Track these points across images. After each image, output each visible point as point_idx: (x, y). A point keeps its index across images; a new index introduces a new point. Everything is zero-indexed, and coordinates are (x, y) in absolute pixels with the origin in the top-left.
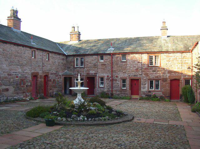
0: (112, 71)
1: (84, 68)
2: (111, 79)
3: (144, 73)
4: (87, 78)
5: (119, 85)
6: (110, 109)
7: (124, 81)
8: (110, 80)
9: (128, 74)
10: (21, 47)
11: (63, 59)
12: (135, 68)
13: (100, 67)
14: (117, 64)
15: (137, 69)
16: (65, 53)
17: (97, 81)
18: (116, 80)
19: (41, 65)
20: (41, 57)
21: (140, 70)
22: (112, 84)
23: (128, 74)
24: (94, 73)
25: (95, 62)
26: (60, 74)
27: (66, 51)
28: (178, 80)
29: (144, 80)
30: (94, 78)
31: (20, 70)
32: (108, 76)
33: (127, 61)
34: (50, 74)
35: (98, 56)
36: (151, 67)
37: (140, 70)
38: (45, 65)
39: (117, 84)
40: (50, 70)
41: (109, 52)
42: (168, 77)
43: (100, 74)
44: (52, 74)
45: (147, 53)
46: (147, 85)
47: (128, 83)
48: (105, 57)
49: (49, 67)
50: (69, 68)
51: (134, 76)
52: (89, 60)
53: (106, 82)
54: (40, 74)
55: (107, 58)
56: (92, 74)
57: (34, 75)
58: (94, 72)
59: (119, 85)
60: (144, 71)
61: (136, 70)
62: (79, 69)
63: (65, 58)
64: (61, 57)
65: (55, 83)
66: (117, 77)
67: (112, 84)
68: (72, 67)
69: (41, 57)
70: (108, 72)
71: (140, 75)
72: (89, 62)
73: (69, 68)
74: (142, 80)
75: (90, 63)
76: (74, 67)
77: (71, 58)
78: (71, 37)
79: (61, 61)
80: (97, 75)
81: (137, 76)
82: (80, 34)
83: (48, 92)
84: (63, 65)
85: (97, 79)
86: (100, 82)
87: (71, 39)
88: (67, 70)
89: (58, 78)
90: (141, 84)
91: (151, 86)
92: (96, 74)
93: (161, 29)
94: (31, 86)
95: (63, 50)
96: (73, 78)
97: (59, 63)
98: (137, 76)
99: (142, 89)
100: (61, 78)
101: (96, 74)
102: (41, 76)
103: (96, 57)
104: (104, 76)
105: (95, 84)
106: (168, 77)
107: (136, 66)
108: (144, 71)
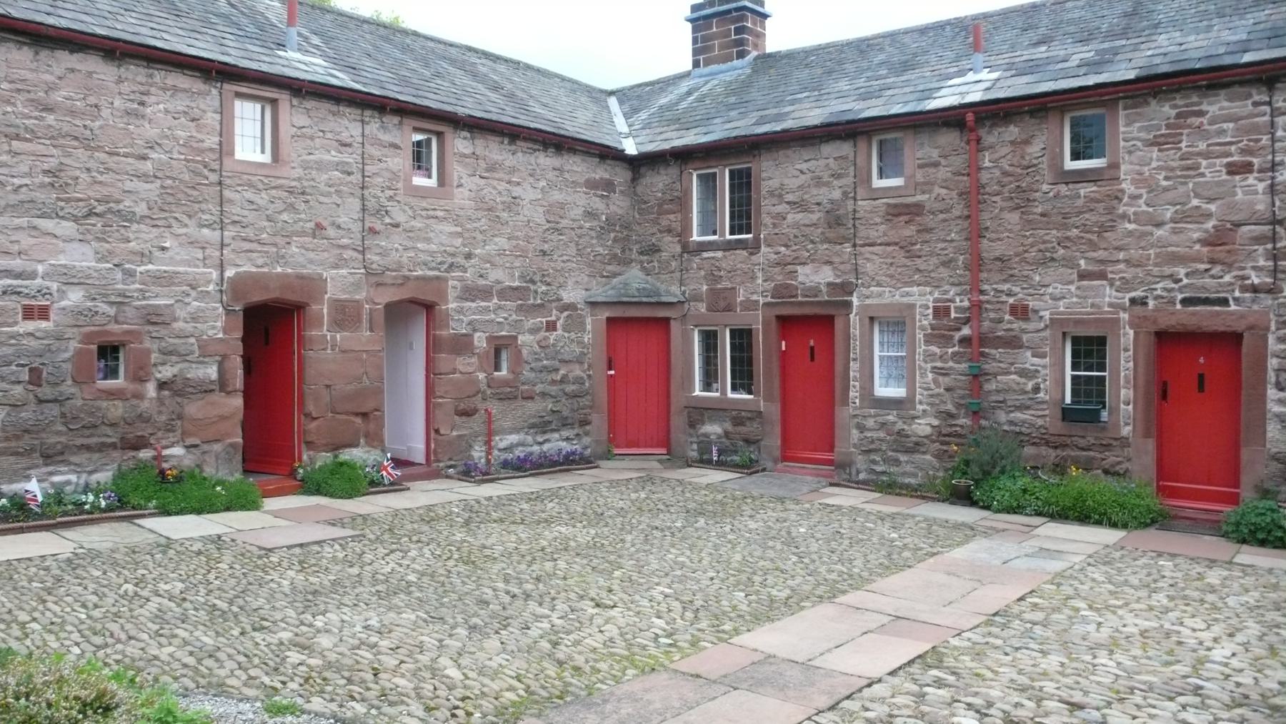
0: (976, 264)
1: (754, 247)
2: (966, 331)
5: (1037, 389)
8: (965, 341)
9: (1126, 285)
10: (91, 64)
11: (609, 186)
12: (1195, 232)
13: (878, 231)
14: (1022, 200)
15: (1217, 240)
18: (1013, 343)
19: (348, 215)
20: (350, 158)
21: (1259, 240)
22: (977, 377)
24: (829, 284)
25: (837, 194)
26: (572, 294)
28: (749, 332)
31: (81, 257)
32: (941, 312)
33: (1114, 166)
34: (451, 294)
35: (862, 144)
37: (1259, 240)
38: (400, 217)
39: (1023, 373)
40: (460, 260)
43: (880, 295)
44: (470, 293)
49: (443, 236)
50: (654, 250)
51: (1185, 302)
52: (792, 183)
53: (929, 357)
54: (332, 292)
55: (935, 154)
56: (815, 291)
58: (826, 276)
59: (1037, 389)
61: (1204, 242)
62: (719, 254)
63: (621, 175)
64: (578, 167)
65: (517, 360)
66: (1021, 312)
67: (977, 377)
68: (671, 246)
69: (350, 158)
70: (944, 273)
71: (1255, 289)
72: (790, 197)
73: (654, 250)
77: (658, 182)
79: (580, 201)
80: (855, 301)
81: (1224, 302)
82: (765, 16)
83: (437, 431)
84: (602, 232)
85: (856, 330)
86: (877, 353)
88: (643, 269)
90: (1263, 382)
92: (846, 288)
94: (223, 384)
97: (555, 212)
98: (1224, 302)
100: (575, 324)
101: (846, 288)
102: (346, 315)
103: (845, 148)
105: (839, 367)
107: (1213, 207)
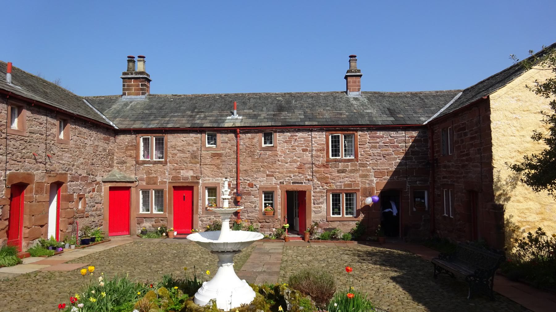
1: (166, 163)
3: (318, 175)
4: (172, 189)
5: (255, 207)
6: (191, 241)
7: (269, 195)
13: (208, 161)
16: (111, 123)
17: (201, 195)
23: (279, 178)
24: (192, 177)
27: (113, 118)
29: (318, 192)
30: (191, 188)
35: (203, 135)
36: (336, 161)
40: (71, 167)
41: (230, 125)
42: (374, 185)
43: (209, 180)
45: (322, 128)
46: (324, 206)
47: (280, 200)
48: (220, 137)
52: (180, 144)
54: (36, 179)
56: (187, 178)
57: (15, 182)
58: (190, 174)
59: (255, 207)
60: (316, 172)
62: (151, 165)
66: (251, 185)
71: (308, 180)
72: (179, 148)
74: (312, 194)
75: (182, 151)
76: (137, 162)
78: (124, 85)
81: (302, 183)
85: (201, 190)
87: (124, 90)
89: (94, 190)
91: (336, 208)
92: (197, 178)
93: (360, 76)
95: (104, 117)
96: (133, 190)
98: (302, 183)
99: (313, 215)
104: (219, 183)
106: (374, 185)
108: (316, 172)
